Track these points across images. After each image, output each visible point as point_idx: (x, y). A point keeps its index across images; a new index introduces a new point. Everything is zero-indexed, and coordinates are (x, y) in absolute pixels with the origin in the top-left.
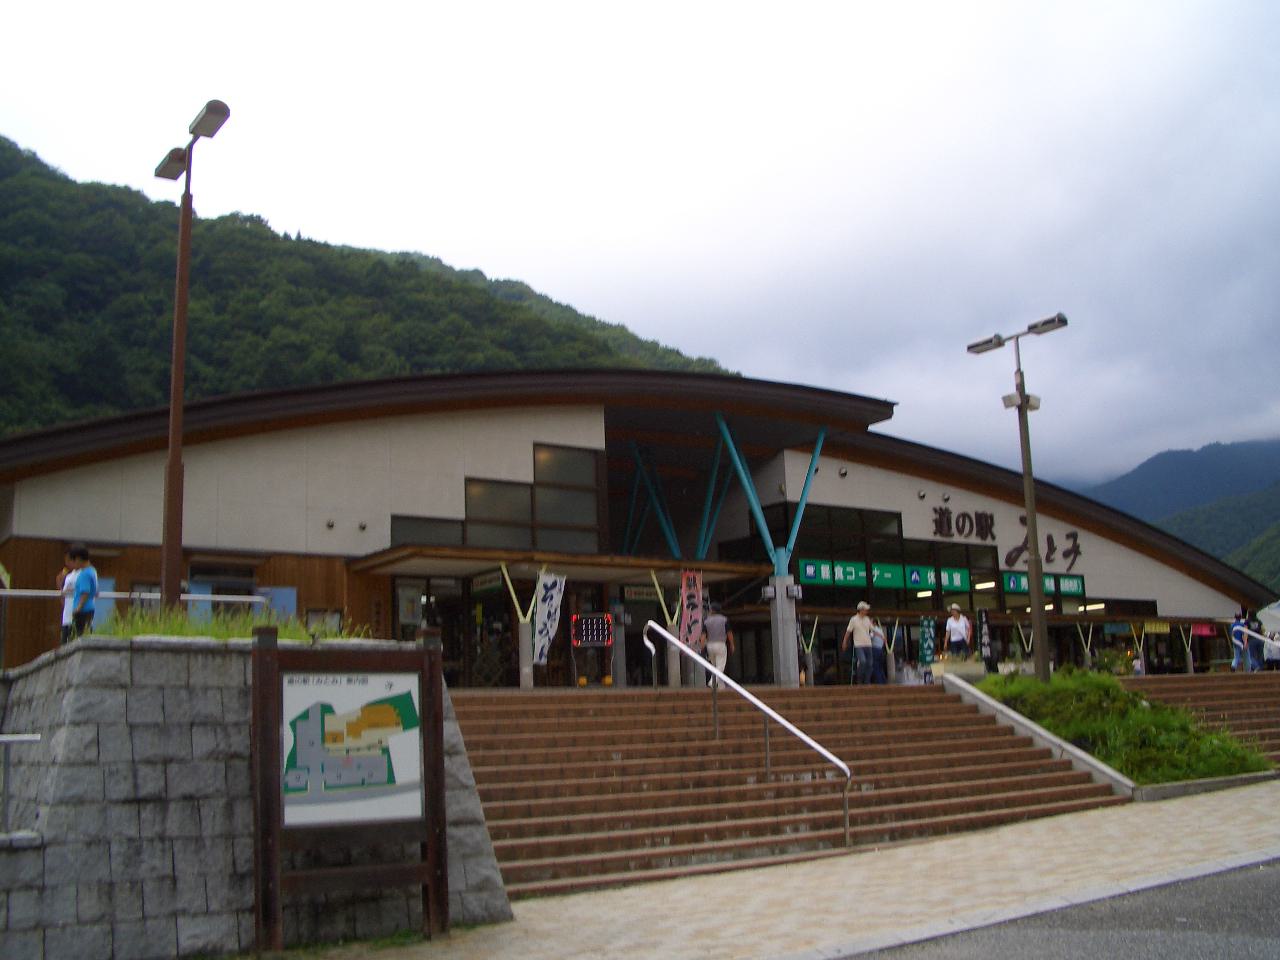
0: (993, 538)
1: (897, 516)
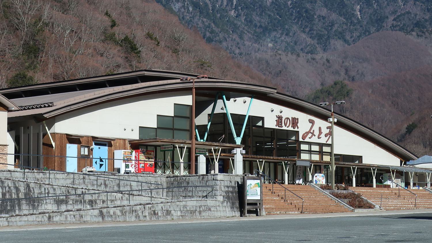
0: (298, 128)
1: (262, 119)
